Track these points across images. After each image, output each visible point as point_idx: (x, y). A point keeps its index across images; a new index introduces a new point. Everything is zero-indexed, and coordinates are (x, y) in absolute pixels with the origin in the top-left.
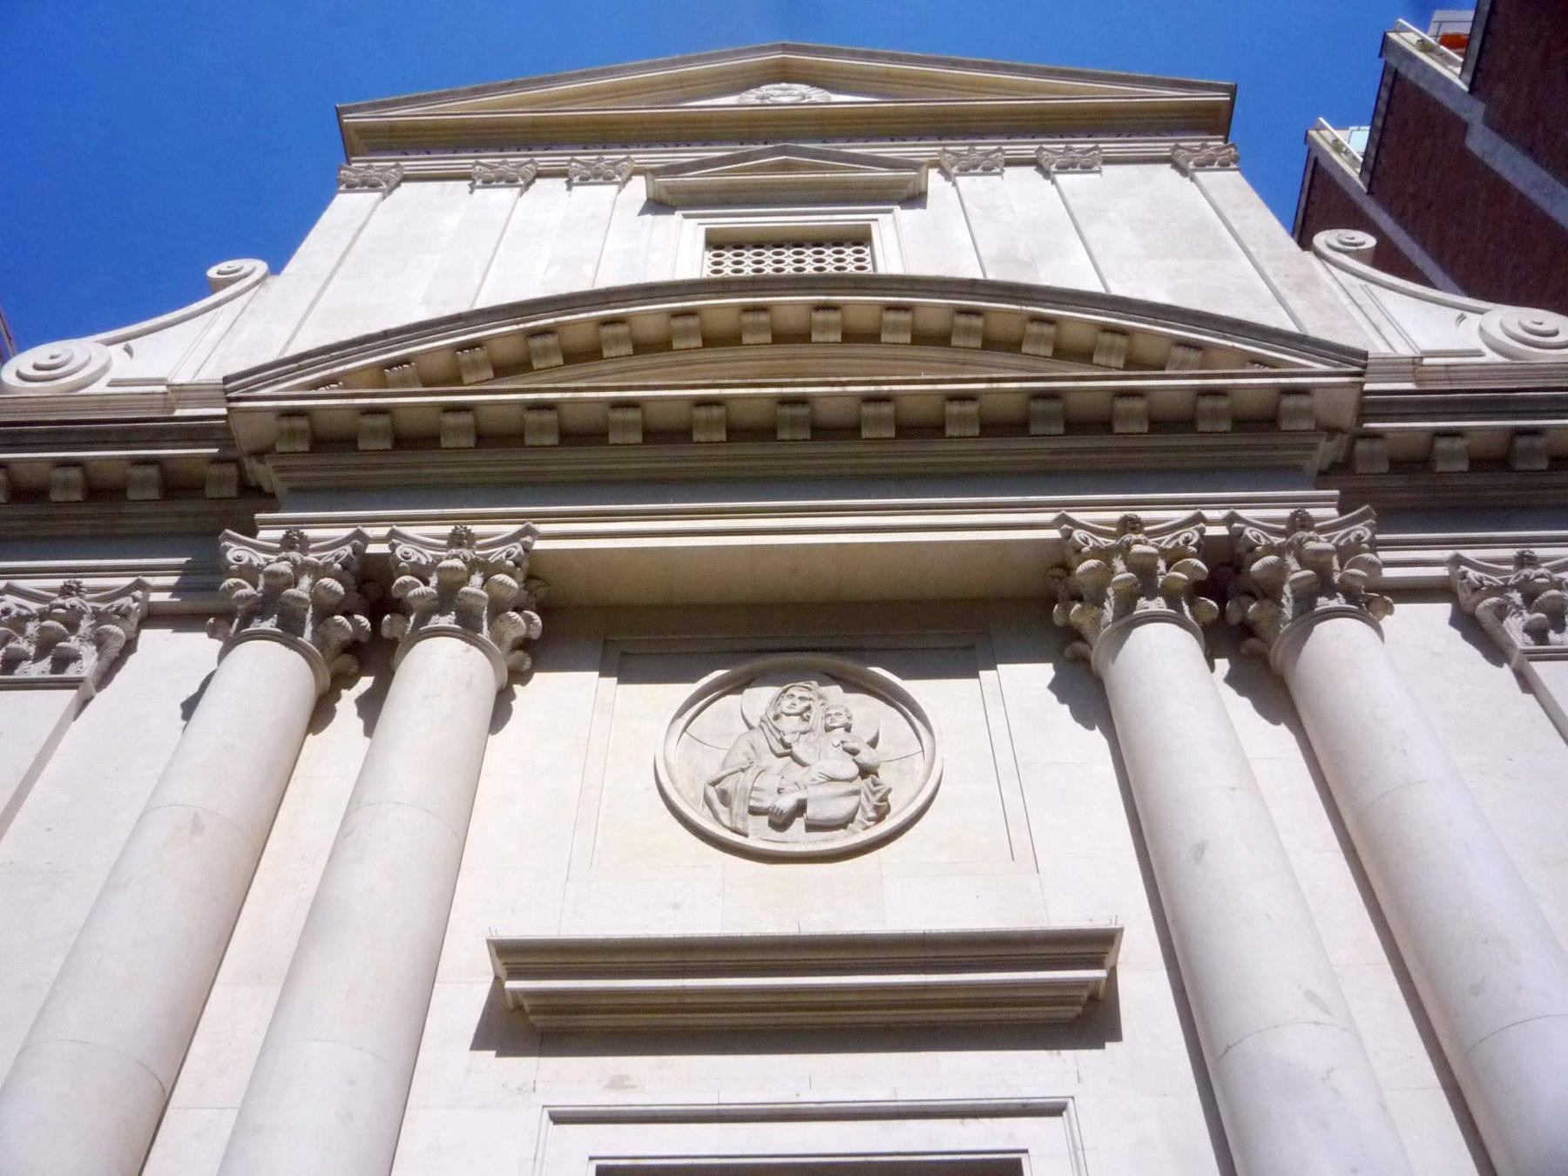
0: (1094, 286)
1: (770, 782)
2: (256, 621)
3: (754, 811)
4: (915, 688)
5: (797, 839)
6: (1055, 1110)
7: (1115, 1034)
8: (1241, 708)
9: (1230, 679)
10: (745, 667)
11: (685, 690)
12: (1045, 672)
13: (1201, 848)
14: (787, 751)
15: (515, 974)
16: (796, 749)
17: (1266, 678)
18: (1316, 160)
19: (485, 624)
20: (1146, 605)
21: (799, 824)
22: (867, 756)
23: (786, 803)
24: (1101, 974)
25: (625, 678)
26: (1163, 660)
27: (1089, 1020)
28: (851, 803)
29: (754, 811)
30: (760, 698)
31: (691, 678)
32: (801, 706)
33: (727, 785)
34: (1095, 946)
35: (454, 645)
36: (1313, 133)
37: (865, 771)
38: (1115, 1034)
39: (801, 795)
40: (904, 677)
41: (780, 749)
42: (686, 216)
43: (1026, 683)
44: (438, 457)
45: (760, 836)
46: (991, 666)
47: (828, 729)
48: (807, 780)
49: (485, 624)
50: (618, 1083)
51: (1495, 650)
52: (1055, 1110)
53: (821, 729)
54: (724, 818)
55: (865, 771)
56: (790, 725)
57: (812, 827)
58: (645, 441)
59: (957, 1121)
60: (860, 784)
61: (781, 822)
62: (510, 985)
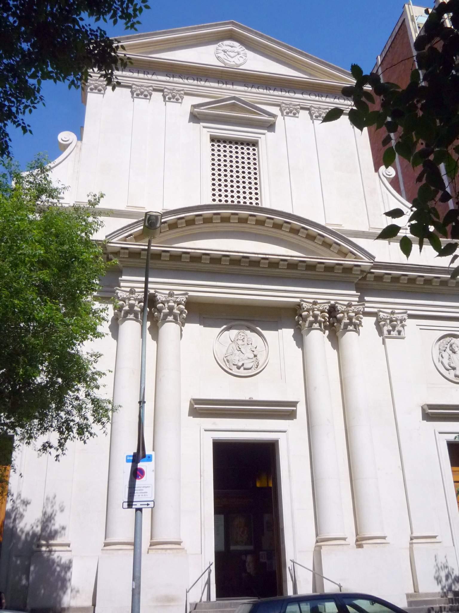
0: (323, 223)
1: (237, 358)
2: (129, 315)
3: (234, 365)
4: (264, 332)
5: (242, 372)
6: (285, 432)
7: (296, 418)
8: (328, 344)
9: (328, 337)
10: (230, 325)
11: (219, 330)
12: (291, 331)
13: (315, 388)
14: (240, 350)
15: (196, 404)
16: (242, 350)
17: (335, 339)
18: (404, 19)
19: (49, 64)
20: (316, 325)
21: (242, 368)
22: (255, 353)
23: (240, 364)
24: (294, 408)
25: (205, 326)
26: (318, 338)
27: (291, 415)
28: (252, 364)
29: (234, 365)
30: (234, 333)
31: (220, 327)
32: (242, 338)
33: (228, 358)
34: (294, 404)
35: (173, 325)
36: (406, 6)
37: (255, 356)
38: (296, 418)
39: (243, 362)
40: (263, 329)
41: (238, 349)
42: (204, 127)
43: (288, 333)
44: (160, 262)
45: (235, 371)
46: (281, 329)
47: (248, 344)
48: (244, 358)
49: (49, 64)
50: (214, 423)
51: (381, 333)
52: (285, 432)
53: (246, 344)
54: (228, 365)
55: (255, 356)
56: (240, 342)
57: (245, 369)
58: (211, 263)
59: (255, 398)
60: (255, 359)
61: (239, 368)
62: (196, 406)
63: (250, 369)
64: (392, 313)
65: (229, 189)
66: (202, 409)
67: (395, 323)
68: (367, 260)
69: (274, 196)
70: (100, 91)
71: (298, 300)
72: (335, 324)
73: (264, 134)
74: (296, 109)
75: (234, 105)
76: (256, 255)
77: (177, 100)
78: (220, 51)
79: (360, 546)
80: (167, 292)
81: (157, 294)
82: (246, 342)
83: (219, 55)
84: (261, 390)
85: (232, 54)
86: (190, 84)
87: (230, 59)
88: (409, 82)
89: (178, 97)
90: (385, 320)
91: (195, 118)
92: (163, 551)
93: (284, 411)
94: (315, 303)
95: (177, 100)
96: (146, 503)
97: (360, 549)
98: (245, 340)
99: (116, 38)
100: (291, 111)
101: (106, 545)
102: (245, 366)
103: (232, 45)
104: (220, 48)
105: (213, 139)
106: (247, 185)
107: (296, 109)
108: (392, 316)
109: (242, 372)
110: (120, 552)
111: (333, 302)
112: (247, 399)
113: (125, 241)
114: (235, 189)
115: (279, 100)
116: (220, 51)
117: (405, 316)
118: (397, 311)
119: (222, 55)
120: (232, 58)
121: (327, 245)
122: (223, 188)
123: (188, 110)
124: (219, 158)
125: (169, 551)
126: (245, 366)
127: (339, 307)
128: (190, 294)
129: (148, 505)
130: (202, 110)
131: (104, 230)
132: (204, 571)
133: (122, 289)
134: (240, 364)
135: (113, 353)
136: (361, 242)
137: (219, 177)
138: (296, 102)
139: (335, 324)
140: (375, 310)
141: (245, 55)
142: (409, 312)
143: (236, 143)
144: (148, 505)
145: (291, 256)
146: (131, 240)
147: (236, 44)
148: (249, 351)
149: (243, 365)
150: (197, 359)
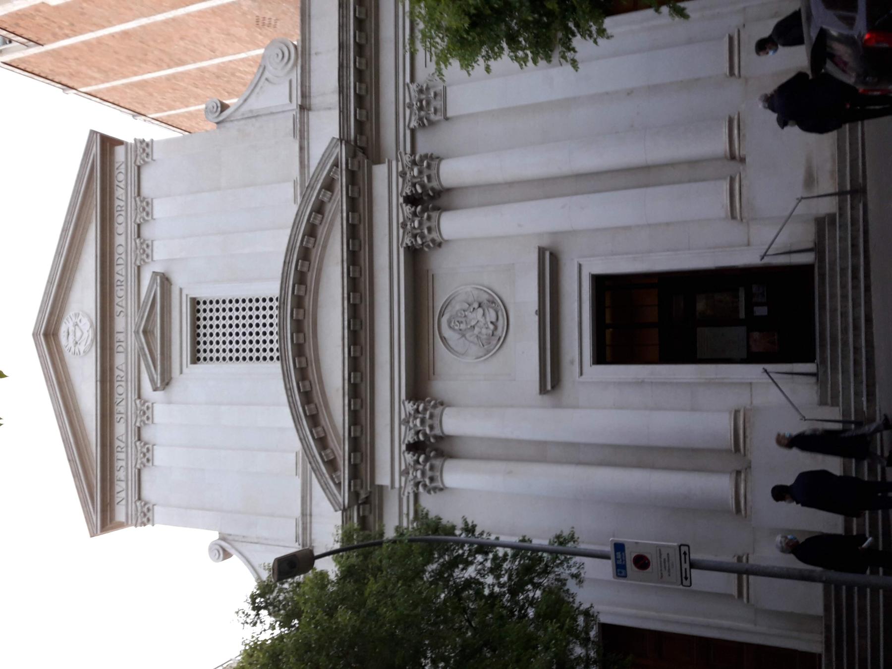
1: (484, 331)
5: (501, 323)
50: (572, 362)
64: (410, 106)
65: (261, 338)
66: (551, 378)
67: (424, 103)
69: (262, 276)
70: (149, 510)
71: (402, 251)
73: (181, 290)
74: (142, 244)
75: (145, 332)
76: (346, 311)
78: (77, 351)
79: (743, 160)
80: (403, 428)
82: (463, 320)
85: (78, 334)
87: (86, 335)
88: (782, 50)
89: (145, 408)
92: (748, 440)
93: (550, 263)
95: (148, 408)
97: (747, 160)
98: (460, 320)
100: (144, 250)
102: (494, 320)
103: (66, 334)
106: (254, 313)
107: (142, 244)
108: (415, 107)
109: (501, 323)
110: (749, 497)
111: (401, 200)
112: (536, 318)
113: (340, 483)
114: (261, 321)
115: (132, 271)
116: (77, 351)
118: (407, 100)
119: (82, 348)
121: (319, 209)
123: (159, 394)
125: (748, 433)
126: (494, 320)
128: (403, 396)
130: (158, 378)
131: (328, 529)
132: (770, 381)
134: (491, 327)
137: (254, 334)
138: (131, 245)
140: (408, 133)
141: (77, 315)
142: (408, 80)
146: (338, 477)
147: (63, 329)
148: (474, 315)
149: (492, 323)
150: (490, 391)
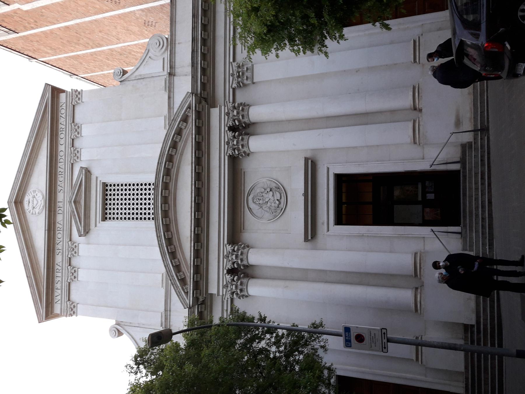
1: (273, 205)
5: (283, 200)
26: (255, 143)
50: (323, 224)
59: (302, 191)
63: (281, 194)
64: (233, 75)
67: (241, 73)
68: (191, 99)
69: (145, 171)
71: (226, 158)
72: (242, 129)
73: (97, 178)
74: (74, 150)
75: (75, 202)
76: (193, 192)
77: (76, 246)
78: (34, 212)
79: (420, 110)
80: (225, 260)
81: (227, 268)
83: (37, 213)
84: (296, 186)
85: (35, 202)
86: (60, 236)
90: (238, 83)
91: (86, 231)
92: (422, 270)
94: (228, 143)
95: (76, 246)
96: (383, 335)
99: (15, 35)
101: (416, 310)
102: (279, 198)
103: (28, 202)
104: (31, 212)
105: (104, 219)
107: (74, 150)
109: (283, 200)
111: (227, 129)
112: (303, 197)
113: (188, 292)
117: (234, 64)
118: (231, 72)
119: (37, 210)
120: (38, 202)
121: (179, 132)
122: (140, 197)
124: (116, 204)
125: (422, 266)
126: (279, 198)
127: (230, 124)
128: (226, 242)
129: (384, 333)
130: (82, 229)
133: (224, 293)
134: (277, 202)
135: (272, 302)
136: (177, 106)
138: (68, 151)
139: (242, 129)
140: (231, 90)
142: (231, 60)
143: (106, 209)
144: (384, 333)
145: (191, 232)
146: (187, 288)
147: (26, 199)
150: (274, 238)
